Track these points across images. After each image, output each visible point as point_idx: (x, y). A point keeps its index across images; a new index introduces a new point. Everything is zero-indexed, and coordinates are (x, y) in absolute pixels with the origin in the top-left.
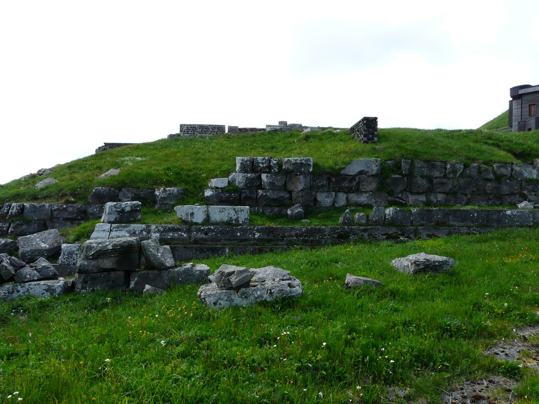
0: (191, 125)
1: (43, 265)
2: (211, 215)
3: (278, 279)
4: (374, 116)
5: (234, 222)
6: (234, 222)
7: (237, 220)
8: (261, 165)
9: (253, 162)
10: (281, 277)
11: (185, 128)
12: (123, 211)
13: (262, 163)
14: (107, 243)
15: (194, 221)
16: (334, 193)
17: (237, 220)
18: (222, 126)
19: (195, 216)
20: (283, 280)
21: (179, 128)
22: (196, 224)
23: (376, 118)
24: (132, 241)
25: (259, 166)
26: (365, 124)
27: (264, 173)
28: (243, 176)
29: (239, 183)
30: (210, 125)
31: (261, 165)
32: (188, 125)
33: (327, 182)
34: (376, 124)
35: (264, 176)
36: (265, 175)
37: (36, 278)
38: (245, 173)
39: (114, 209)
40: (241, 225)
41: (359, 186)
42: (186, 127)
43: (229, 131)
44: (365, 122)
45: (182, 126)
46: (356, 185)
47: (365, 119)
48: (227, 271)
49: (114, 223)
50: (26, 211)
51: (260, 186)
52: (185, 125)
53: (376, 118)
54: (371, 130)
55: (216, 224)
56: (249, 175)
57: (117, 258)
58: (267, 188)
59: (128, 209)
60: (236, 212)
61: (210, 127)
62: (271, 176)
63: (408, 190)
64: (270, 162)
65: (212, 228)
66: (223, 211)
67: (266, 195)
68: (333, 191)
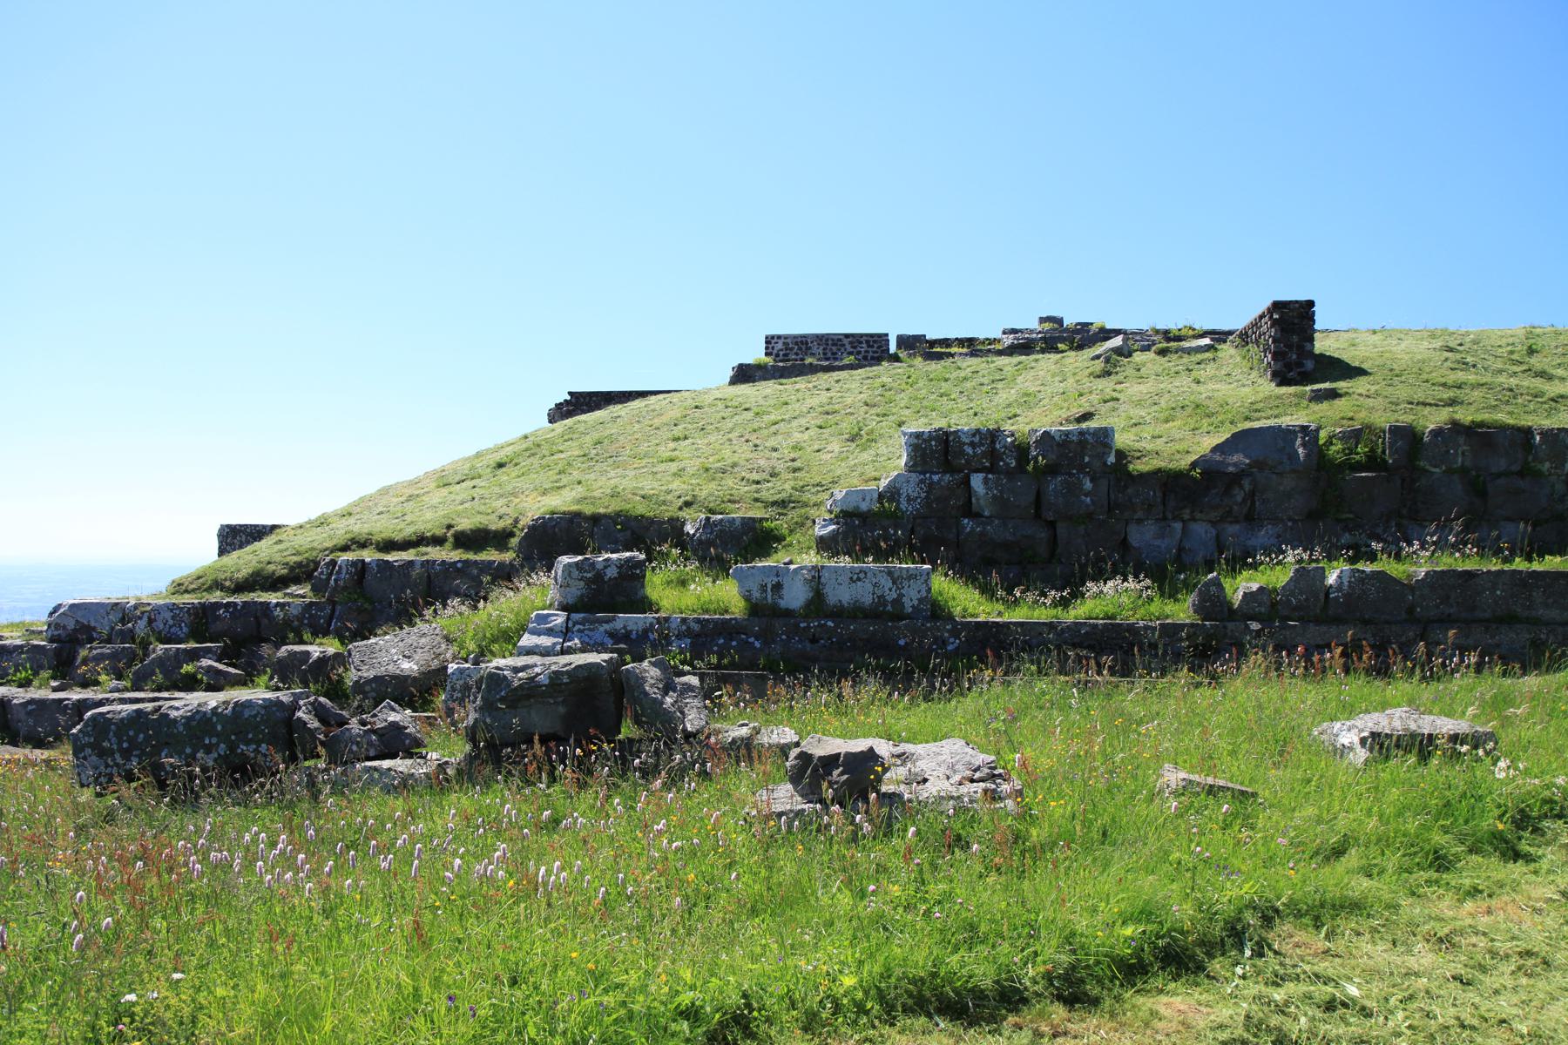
0: (795, 337)
1: (390, 719)
2: (828, 590)
3: (957, 778)
4: (1302, 297)
5: (889, 608)
6: (889, 608)
7: (898, 602)
8: (969, 450)
9: (947, 442)
10: (969, 773)
11: (780, 346)
12: (599, 577)
13: (972, 444)
14: (537, 670)
15: (783, 604)
16: (1178, 526)
17: (898, 602)
18: (879, 335)
19: (784, 592)
20: (972, 781)
21: (314, 514)
22: (788, 613)
23: (1311, 304)
24: (597, 665)
25: (963, 453)
26: (1275, 323)
27: (977, 471)
28: (921, 481)
29: (909, 499)
30: (847, 336)
31: (969, 450)
32: (786, 337)
33: (1159, 494)
34: (1310, 318)
35: (977, 481)
36: (981, 475)
37: (372, 753)
38: (924, 473)
39: (576, 573)
40: (908, 617)
41: (1253, 502)
42: (781, 342)
43: (899, 346)
44: (1276, 316)
45: (769, 340)
46: (1244, 500)
47: (1277, 306)
48: (819, 751)
49: (577, 611)
50: (368, 577)
51: (968, 510)
52: (779, 337)
53: (1311, 304)
54: (1295, 338)
55: (839, 613)
56: (936, 478)
57: (562, 710)
58: (987, 513)
59: (612, 573)
60: (894, 583)
61: (846, 341)
62: (998, 479)
63: (1404, 512)
64: (993, 442)
65: (830, 624)
66: (859, 579)
67: (982, 534)
68: (1175, 518)
